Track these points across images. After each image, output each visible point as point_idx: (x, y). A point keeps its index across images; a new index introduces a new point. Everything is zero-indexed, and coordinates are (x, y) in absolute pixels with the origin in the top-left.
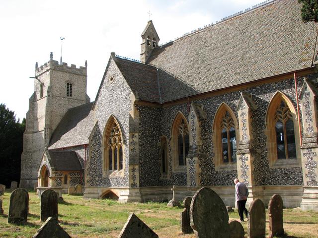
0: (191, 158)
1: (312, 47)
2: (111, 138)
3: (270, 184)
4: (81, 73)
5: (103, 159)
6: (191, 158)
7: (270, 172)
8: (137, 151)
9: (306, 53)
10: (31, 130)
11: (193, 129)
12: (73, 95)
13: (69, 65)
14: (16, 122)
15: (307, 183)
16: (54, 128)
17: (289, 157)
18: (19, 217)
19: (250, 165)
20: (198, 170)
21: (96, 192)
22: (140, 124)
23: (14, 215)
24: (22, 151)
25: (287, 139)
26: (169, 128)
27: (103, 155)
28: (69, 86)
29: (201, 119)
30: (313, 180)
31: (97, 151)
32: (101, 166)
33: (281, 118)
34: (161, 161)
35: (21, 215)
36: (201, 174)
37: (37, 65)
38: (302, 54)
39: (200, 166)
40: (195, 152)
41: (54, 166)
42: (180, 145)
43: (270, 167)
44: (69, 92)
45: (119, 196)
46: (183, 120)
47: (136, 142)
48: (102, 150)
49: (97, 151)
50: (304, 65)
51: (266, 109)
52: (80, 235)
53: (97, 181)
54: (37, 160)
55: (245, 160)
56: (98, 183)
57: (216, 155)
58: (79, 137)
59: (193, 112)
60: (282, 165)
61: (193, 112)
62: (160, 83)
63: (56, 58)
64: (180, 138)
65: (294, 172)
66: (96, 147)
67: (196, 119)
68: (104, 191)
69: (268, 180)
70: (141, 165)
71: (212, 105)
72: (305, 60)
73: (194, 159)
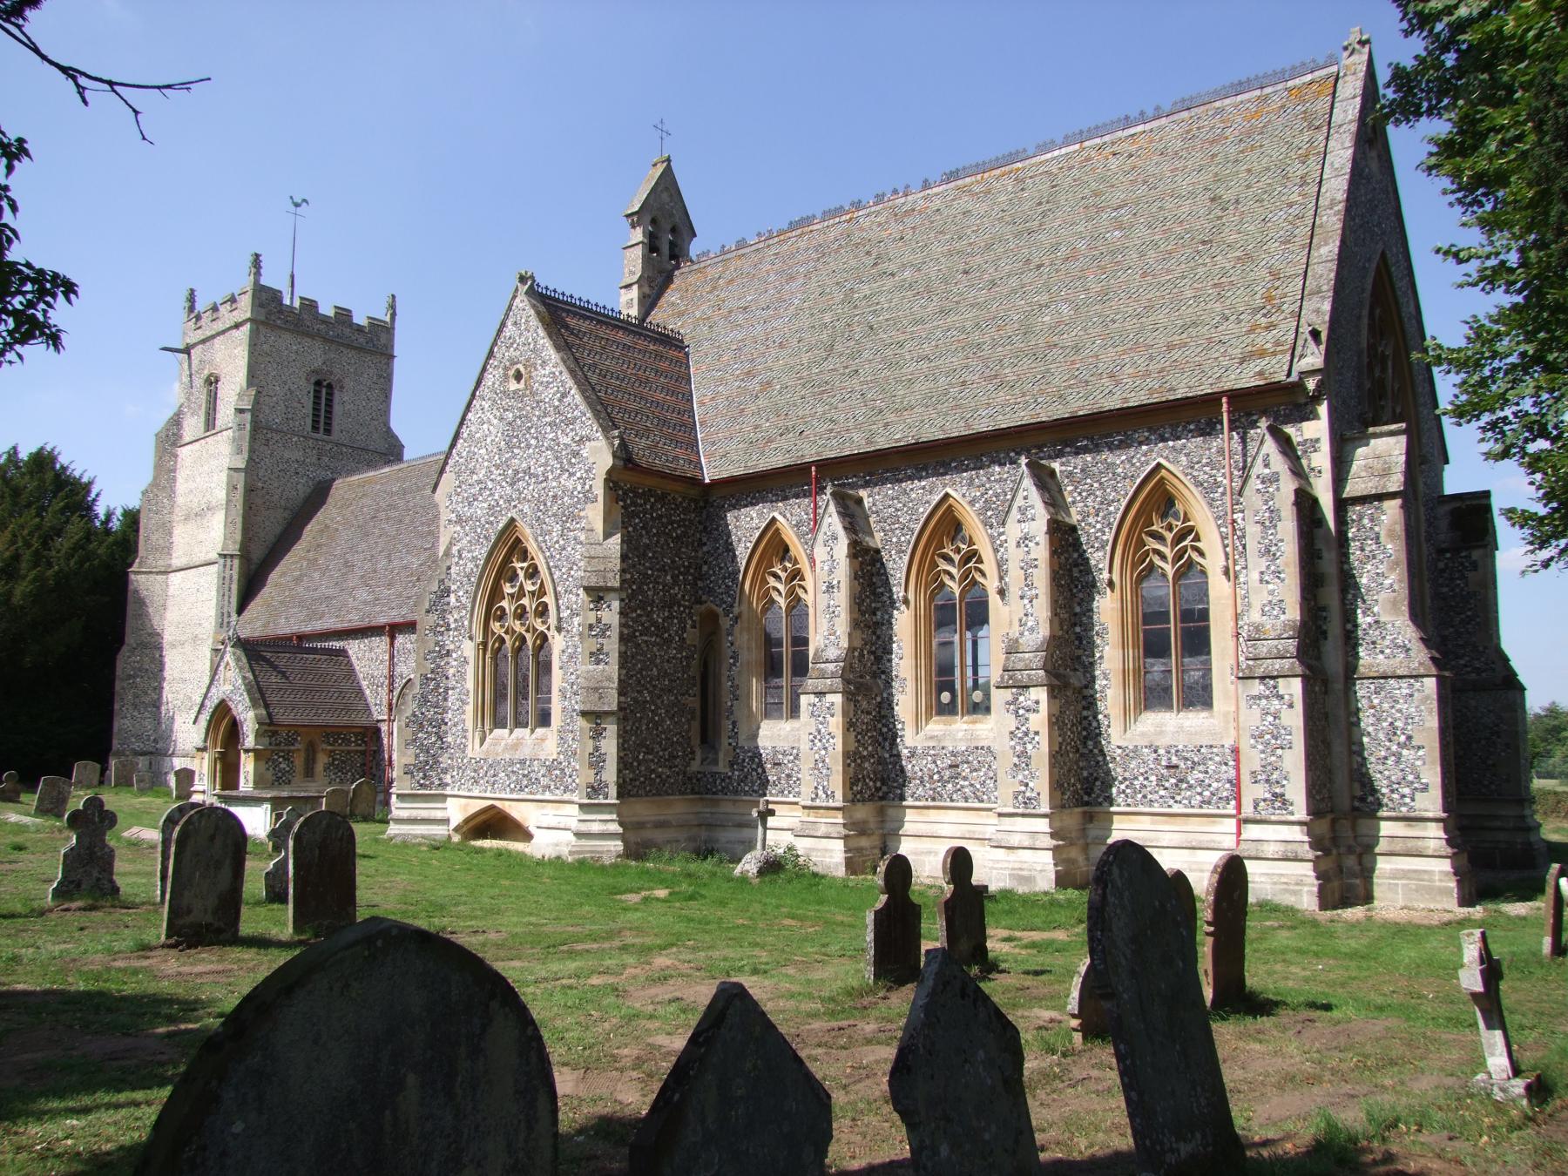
8: (614, 659)
9: (1270, 327)
11: (830, 587)
19: (1044, 731)
30: (1275, 795)
50: (1261, 373)
58: (362, 594)
65: (1203, 762)
72: (1262, 354)
73: (830, 698)
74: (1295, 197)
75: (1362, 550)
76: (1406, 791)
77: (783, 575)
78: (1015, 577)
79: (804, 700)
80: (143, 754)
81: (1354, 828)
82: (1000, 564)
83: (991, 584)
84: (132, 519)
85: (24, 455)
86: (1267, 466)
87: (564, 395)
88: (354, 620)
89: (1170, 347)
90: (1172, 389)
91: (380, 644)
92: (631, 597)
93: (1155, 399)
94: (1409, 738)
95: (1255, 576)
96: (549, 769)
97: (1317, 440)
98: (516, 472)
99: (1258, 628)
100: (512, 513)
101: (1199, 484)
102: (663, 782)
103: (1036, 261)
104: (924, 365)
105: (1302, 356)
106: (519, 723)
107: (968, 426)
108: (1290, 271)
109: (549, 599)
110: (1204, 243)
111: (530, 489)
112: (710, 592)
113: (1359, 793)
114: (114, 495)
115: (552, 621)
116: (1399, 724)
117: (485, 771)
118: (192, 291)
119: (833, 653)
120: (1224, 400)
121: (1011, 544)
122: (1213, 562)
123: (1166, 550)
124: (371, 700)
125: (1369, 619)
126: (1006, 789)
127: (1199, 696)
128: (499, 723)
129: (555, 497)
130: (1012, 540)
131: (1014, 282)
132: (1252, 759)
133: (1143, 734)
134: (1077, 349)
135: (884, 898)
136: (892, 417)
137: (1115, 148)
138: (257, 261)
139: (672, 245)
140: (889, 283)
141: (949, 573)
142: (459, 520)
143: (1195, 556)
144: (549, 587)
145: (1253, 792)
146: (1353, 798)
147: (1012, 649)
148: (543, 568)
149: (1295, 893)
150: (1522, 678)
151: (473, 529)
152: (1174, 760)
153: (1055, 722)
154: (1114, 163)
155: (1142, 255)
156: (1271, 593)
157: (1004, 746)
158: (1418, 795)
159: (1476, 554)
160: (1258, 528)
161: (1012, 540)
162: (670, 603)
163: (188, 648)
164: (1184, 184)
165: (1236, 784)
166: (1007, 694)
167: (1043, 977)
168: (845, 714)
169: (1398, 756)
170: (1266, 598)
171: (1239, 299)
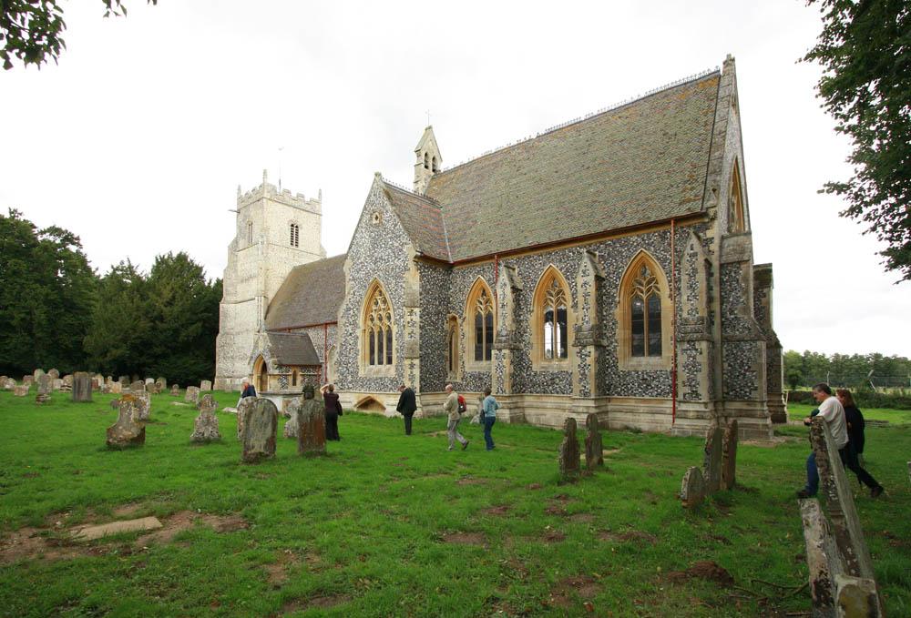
0: (500, 350)
1: (700, 180)
2: (373, 314)
3: (619, 394)
4: (312, 208)
5: (359, 347)
6: (500, 350)
7: (619, 376)
8: (418, 336)
9: (692, 189)
10: (234, 299)
11: (503, 305)
12: (300, 242)
13: (294, 195)
14: (206, 284)
15: (684, 395)
16: (271, 296)
17: (650, 354)
18: (262, 450)
19: (593, 365)
20: (508, 369)
21: (348, 400)
22: (421, 294)
23: (253, 447)
24: (218, 332)
25: (649, 326)
26: (462, 302)
27: (359, 342)
28: (294, 228)
29: (515, 289)
30: (693, 391)
31: (351, 334)
32: (356, 358)
33: (642, 292)
34: (447, 354)
35: (265, 447)
36: (513, 375)
37: (239, 189)
38: (684, 191)
39: (512, 362)
40: (505, 342)
41: (277, 357)
42: (479, 329)
43: (620, 368)
44: (294, 240)
45: (385, 406)
46: (484, 291)
47: (415, 322)
48: (359, 332)
49: (351, 334)
50: (689, 209)
51: (620, 278)
52: (757, 616)
53: (350, 383)
54: (243, 347)
55: (586, 356)
56: (351, 386)
57: (535, 346)
58: (314, 312)
59: (504, 277)
60: (640, 365)
61: (504, 277)
62: (448, 231)
63: (272, 180)
64: (478, 318)
65: (658, 377)
66: (350, 328)
67: (508, 290)
68: (360, 399)
69: (616, 387)
70: (422, 358)
71: (532, 268)
72: (689, 200)
73: (504, 351)
74: (702, 131)
75: (730, 286)
76: (748, 390)
77: (482, 301)
78: (580, 299)
79: (493, 352)
80: (228, 377)
81: (723, 406)
82: (574, 295)
84: (220, 284)
85: (175, 255)
86: (692, 249)
87: (396, 225)
88: (311, 321)
89: (647, 200)
90: (649, 218)
91: (321, 332)
92: (424, 310)
93: (642, 222)
94: (749, 367)
95: (685, 298)
96: (392, 381)
97: (713, 238)
98: (376, 259)
99: (686, 320)
100: (375, 276)
101: (658, 259)
102: (436, 386)
103: (587, 166)
104: (540, 212)
105: (708, 201)
106: (380, 363)
107: (560, 237)
108: (701, 164)
109: (391, 312)
110: (661, 154)
111: (382, 266)
112: (453, 308)
113: (726, 391)
114: (211, 275)
115: (392, 320)
116: (745, 361)
117: (365, 383)
118: (239, 187)
119: (504, 333)
120: (672, 222)
121: (579, 285)
123: (644, 289)
124: (318, 354)
125: (732, 316)
126: (577, 387)
127: (656, 350)
128: (372, 363)
129: (393, 268)
131: (577, 175)
132: (683, 375)
133: (632, 366)
134: (606, 203)
135: (566, 438)
136: (527, 234)
137: (620, 115)
139: (434, 165)
140: (524, 178)
141: (551, 300)
142: (354, 279)
144: (391, 308)
145: (682, 390)
146: (723, 393)
147: (579, 330)
148: (388, 300)
149: (702, 433)
150: (782, 343)
151: (359, 283)
152: (645, 376)
153: (597, 361)
154: (619, 121)
155: (633, 160)
156: (692, 305)
157: (576, 370)
158: (753, 392)
159: (765, 291)
160: (687, 277)
162: (438, 313)
163: (245, 334)
164: (651, 128)
165: (674, 386)
167: (211, 448)
168: (510, 358)
169: (745, 375)
170: (689, 307)
171: (678, 178)
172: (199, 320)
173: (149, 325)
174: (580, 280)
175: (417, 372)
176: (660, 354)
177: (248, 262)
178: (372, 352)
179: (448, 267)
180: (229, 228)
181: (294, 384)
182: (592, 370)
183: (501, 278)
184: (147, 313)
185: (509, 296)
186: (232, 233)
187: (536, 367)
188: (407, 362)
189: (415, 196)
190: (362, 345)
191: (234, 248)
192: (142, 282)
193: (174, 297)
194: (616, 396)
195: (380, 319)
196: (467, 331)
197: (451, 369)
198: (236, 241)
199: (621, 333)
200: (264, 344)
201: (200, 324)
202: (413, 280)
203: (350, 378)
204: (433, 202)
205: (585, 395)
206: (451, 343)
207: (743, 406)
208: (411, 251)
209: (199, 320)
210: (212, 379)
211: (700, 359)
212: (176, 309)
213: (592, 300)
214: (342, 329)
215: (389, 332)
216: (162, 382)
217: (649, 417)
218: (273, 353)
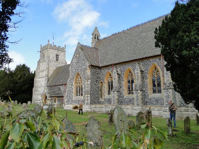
13: (57, 46)
16: (49, 76)
20: (116, 97)
24: (33, 87)
28: (57, 56)
34: (100, 93)
59: (115, 71)
61: (115, 71)
63: (51, 43)
64: (109, 82)
67: (116, 75)
83: (134, 78)
85: (22, 65)
114: (32, 70)
122: (161, 75)
126: (135, 103)
127: (160, 91)
128: (77, 96)
130: (137, 73)
138: (49, 41)
139: (98, 38)
143: (159, 74)
157: (135, 98)
161: (137, 73)
166: (135, 91)
172: (28, 83)
173: (13, 85)
174: (136, 72)
175: (89, 98)
176: (161, 92)
177: (44, 66)
178: (77, 92)
179: (100, 68)
180: (38, 57)
181: (55, 102)
182: (140, 98)
183: (114, 71)
184: (13, 82)
185: (117, 76)
186: (38, 58)
187: (125, 97)
188: (86, 95)
189: (91, 48)
190: (74, 90)
191: (39, 62)
192: (12, 73)
193: (21, 77)
194: (148, 105)
195: (79, 83)
196: (106, 86)
197: (101, 97)
198: (40, 60)
199: (150, 86)
200: (46, 91)
201: (28, 85)
202: (89, 72)
203: (70, 100)
204: (97, 49)
205: (138, 105)
206: (101, 90)
207: (186, 108)
208: (88, 64)
209: (28, 83)
210: (31, 101)
211: (170, 94)
212: (21, 80)
213: (140, 78)
214: (68, 85)
215: (82, 87)
216: (16, 102)
217: (158, 112)
218: (49, 93)
